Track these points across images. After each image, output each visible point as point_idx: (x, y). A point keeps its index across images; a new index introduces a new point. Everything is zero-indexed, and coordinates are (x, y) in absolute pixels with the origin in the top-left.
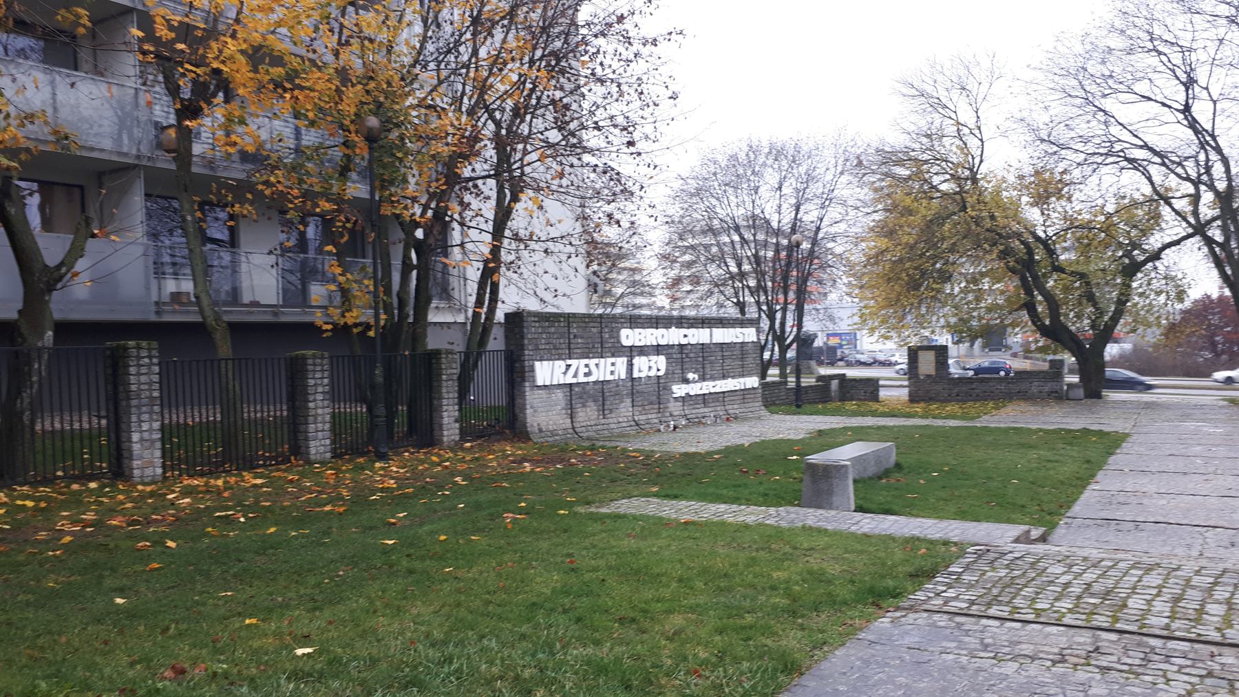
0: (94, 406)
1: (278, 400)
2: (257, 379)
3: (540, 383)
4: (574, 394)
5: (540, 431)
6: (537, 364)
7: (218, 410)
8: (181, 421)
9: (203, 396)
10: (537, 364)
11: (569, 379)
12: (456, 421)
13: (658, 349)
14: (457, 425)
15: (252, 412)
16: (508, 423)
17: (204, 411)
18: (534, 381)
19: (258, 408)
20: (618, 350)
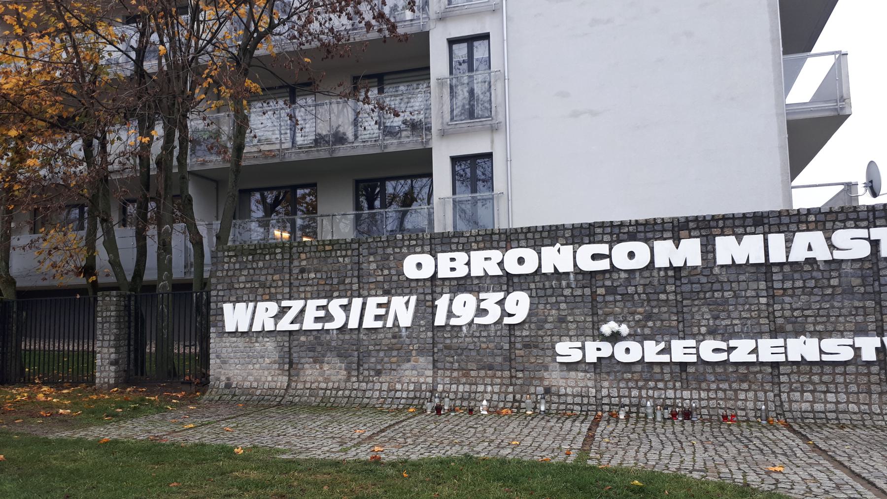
0: (182, 338)
1: (76, 336)
2: (77, 321)
3: (229, 327)
4: (295, 348)
5: (228, 386)
6: (227, 307)
7: (153, 345)
8: (42, 348)
9: (52, 333)
10: (227, 307)
11: (285, 325)
12: (112, 364)
13: (508, 282)
14: (113, 368)
15: (179, 349)
16: (187, 376)
17: (81, 343)
18: (223, 326)
19: (187, 343)
20: (399, 285)
